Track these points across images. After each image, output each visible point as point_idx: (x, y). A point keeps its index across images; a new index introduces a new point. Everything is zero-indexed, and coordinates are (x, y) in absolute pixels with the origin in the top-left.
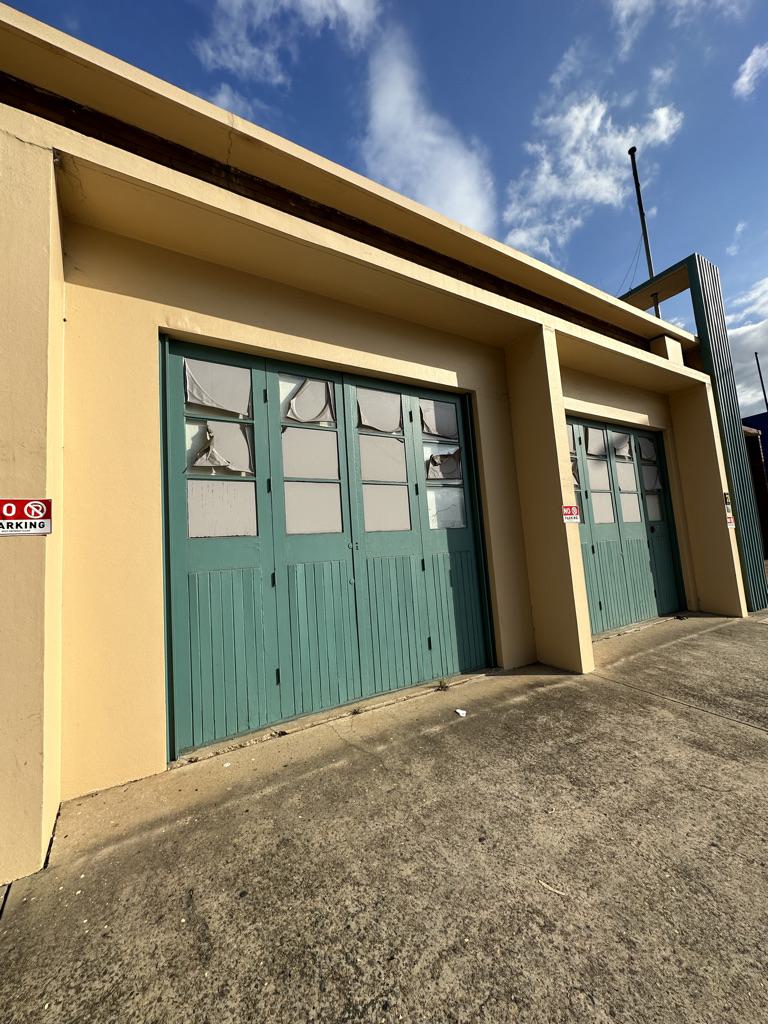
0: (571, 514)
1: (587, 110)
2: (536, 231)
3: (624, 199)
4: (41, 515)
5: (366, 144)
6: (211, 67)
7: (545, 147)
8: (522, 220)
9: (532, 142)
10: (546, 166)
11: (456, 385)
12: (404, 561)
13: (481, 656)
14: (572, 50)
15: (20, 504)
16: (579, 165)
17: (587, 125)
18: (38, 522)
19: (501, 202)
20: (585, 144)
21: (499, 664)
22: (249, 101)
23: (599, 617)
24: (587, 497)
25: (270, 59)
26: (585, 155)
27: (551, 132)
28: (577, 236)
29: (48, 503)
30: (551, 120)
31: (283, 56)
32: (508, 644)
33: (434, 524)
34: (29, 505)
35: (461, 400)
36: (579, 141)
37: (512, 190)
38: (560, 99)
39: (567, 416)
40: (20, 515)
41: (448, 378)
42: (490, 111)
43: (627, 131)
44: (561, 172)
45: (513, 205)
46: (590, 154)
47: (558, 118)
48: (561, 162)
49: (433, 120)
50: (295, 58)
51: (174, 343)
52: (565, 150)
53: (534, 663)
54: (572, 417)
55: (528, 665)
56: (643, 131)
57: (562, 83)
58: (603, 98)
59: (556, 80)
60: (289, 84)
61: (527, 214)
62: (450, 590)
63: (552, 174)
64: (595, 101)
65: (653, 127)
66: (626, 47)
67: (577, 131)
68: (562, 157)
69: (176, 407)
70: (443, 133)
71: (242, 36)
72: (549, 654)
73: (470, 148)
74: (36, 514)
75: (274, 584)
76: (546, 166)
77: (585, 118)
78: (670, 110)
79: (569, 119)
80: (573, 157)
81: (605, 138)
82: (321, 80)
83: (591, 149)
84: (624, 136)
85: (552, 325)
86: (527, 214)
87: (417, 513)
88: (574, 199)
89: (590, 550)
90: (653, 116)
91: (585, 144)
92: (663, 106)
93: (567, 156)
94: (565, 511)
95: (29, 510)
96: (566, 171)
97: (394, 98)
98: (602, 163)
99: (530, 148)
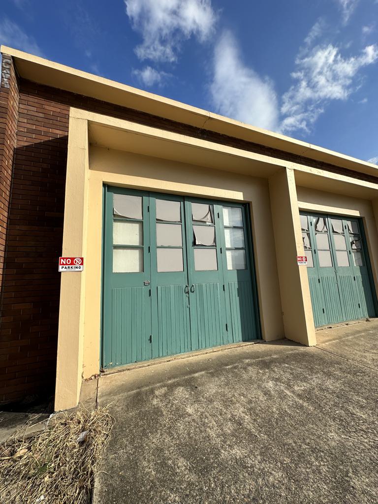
0: (302, 260)
1: (326, 53)
2: (299, 117)
3: (348, 96)
4: (80, 263)
5: (213, 86)
6: (143, 58)
7: (303, 74)
8: (291, 111)
9: (296, 72)
10: (304, 84)
11: (243, 199)
12: (215, 286)
13: (253, 332)
14: (317, 24)
15: (73, 259)
16: (322, 80)
17: (327, 60)
18: (78, 266)
19: (280, 103)
20: (326, 69)
21: (263, 338)
22: (159, 73)
23: (323, 318)
24: (315, 253)
25: (168, 50)
26: (326, 75)
27: (306, 66)
28: (321, 118)
29: (82, 259)
30: (306, 60)
31: (174, 49)
32: (267, 328)
33: (230, 267)
34: (75, 259)
35: (245, 207)
36: (322, 68)
37: (285, 97)
38: (311, 49)
39: (300, 211)
40: (72, 264)
41: (238, 196)
42: (272, 61)
43: (349, 60)
44: (312, 85)
45: (286, 104)
46: (328, 74)
47: (310, 59)
48: (312, 81)
49: (245, 71)
50: (179, 49)
51: (109, 187)
52: (315, 73)
53: (282, 339)
54: (303, 212)
55: (276, 340)
56: (358, 59)
57: (311, 42)
58: (334, 46)
59: (308, 40)
60: (177, 60)
61: (295, 108)
62: (238, 298)
63: (307, 87)
64: (330, 48)
65: (364, 57)
66: (346, 19)
67: (320, 64)
68: (313, 76)
69: (109, 216)
70: (250, 76)
71: (157, 42)
72: (291, 334)
73: (264, 81)
74: (78, 263)
75: (150, 295)
76: (304, 84)
77: (325, 56)
78: (375, 47)
79: (315, 59)
80: (318, 77)
81: (336, 65)
82: (190, 61)
83: (328, 71)
84: (348, 63)
85: (291, 167)
86: (295, 108)
87: (221, 261)
88: (319, 98)
89: (317, 281)
90: (364, 51)
91: (326, 69)
92: (371, 45)
93: (315, 77)
94: (298, 259)
95: (76, 261)
96: (315, 84)
97: (227, 64)
98: (335, 78)
99: (294, 75)
